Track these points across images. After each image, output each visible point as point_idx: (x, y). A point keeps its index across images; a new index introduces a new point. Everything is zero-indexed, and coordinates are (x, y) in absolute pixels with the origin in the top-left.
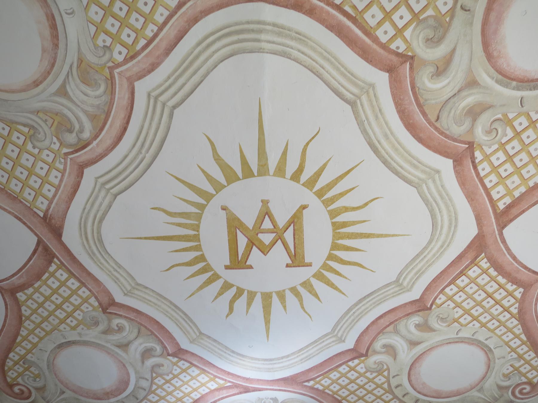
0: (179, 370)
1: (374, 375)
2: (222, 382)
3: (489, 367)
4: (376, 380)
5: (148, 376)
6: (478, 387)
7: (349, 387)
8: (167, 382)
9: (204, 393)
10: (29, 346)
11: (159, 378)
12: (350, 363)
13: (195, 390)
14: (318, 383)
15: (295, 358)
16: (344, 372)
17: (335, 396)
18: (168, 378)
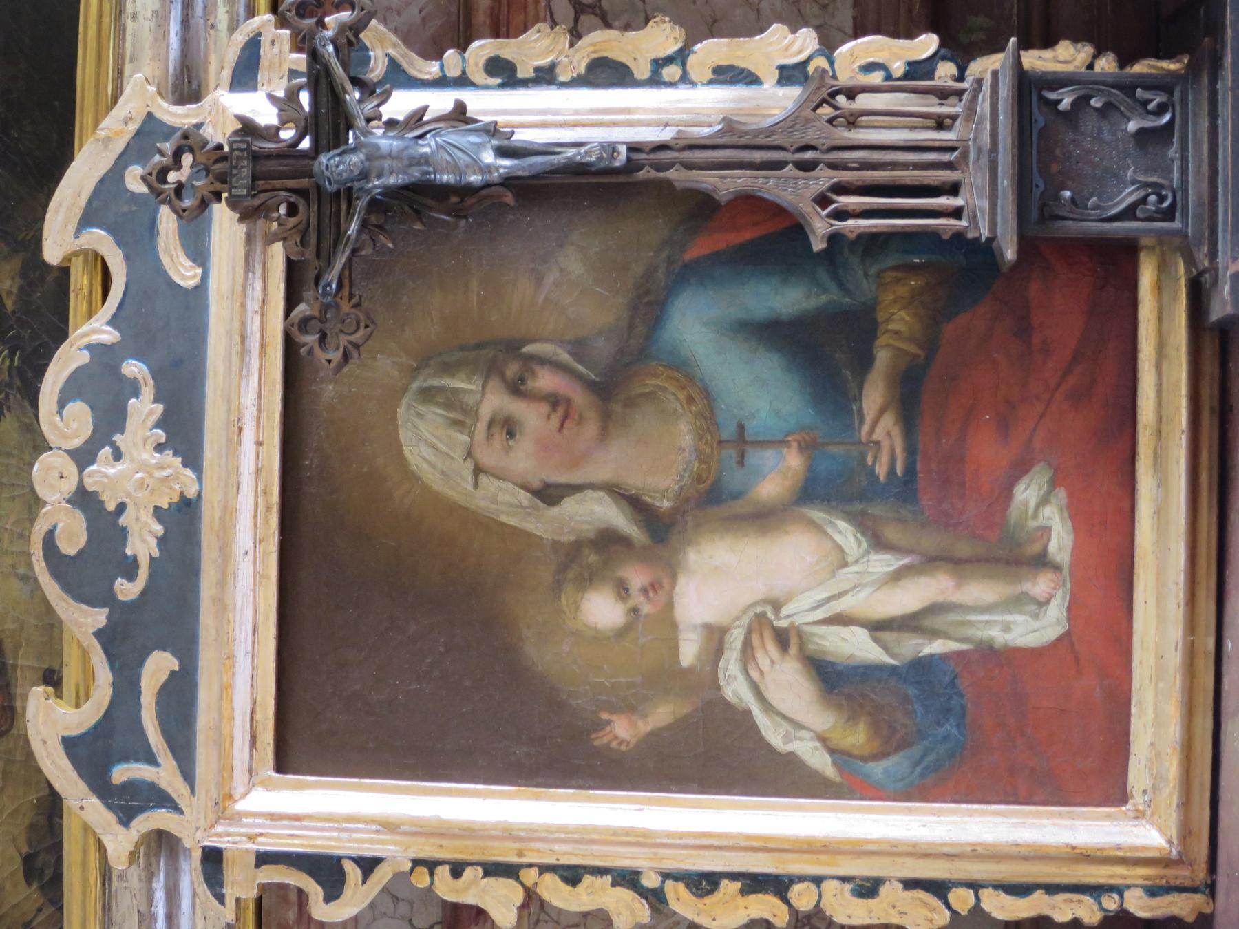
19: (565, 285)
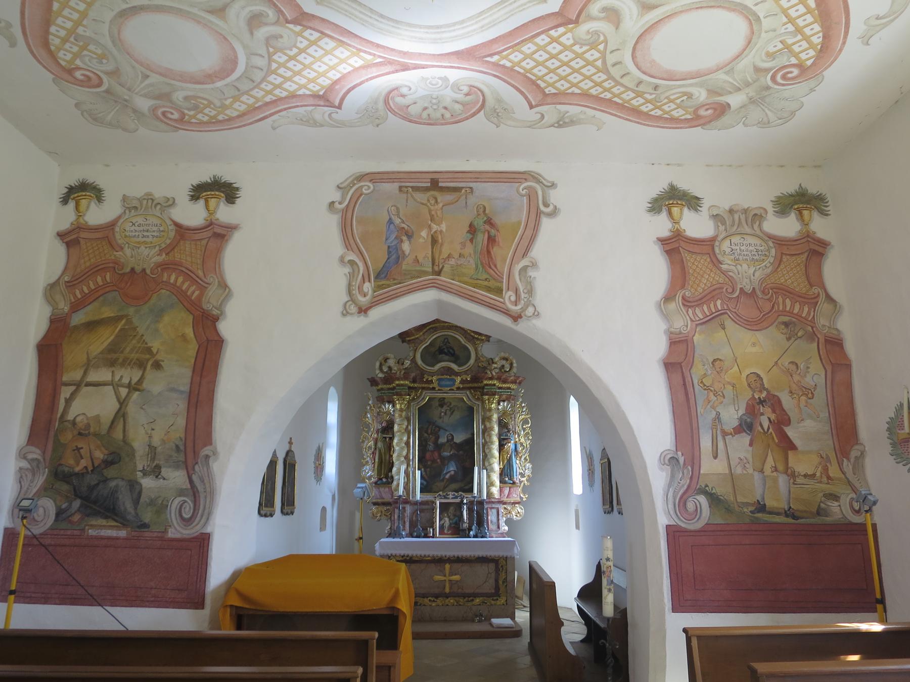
0: (306, 43)
1: (585, 48)
2: (369, 57)
3: (749, 42)
4: (587, 56)
5: (263, 51)
6: (728, 68)
7: (548, 64)
8: (291, 58)
9: (345, 72)
10: (75, 16)
11: (279, 54)
12: (552, 32)
13: (333, 68)
14: (506, 58)
15: (472, 24)
16: (542, 43)
17: (528, 75)
18: (291, 53)
19: (458, 513)
